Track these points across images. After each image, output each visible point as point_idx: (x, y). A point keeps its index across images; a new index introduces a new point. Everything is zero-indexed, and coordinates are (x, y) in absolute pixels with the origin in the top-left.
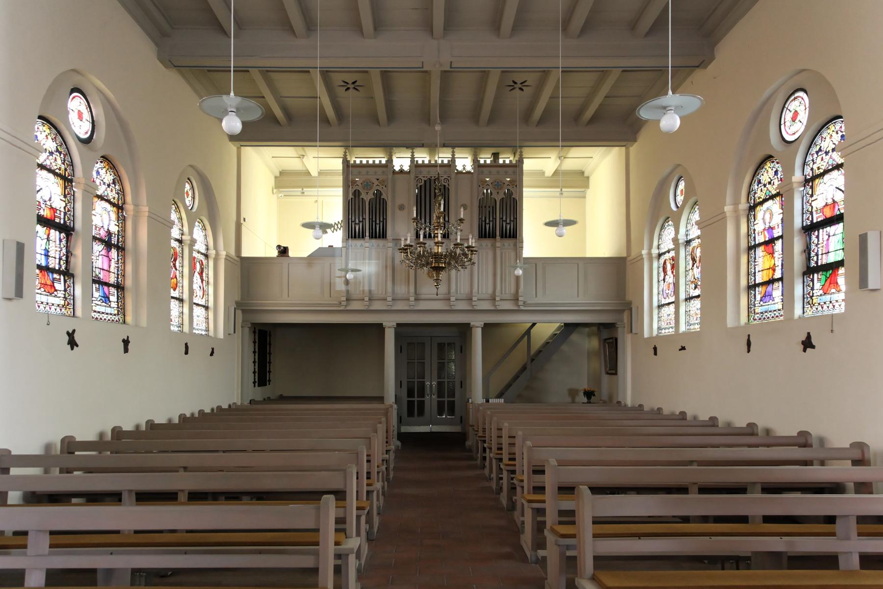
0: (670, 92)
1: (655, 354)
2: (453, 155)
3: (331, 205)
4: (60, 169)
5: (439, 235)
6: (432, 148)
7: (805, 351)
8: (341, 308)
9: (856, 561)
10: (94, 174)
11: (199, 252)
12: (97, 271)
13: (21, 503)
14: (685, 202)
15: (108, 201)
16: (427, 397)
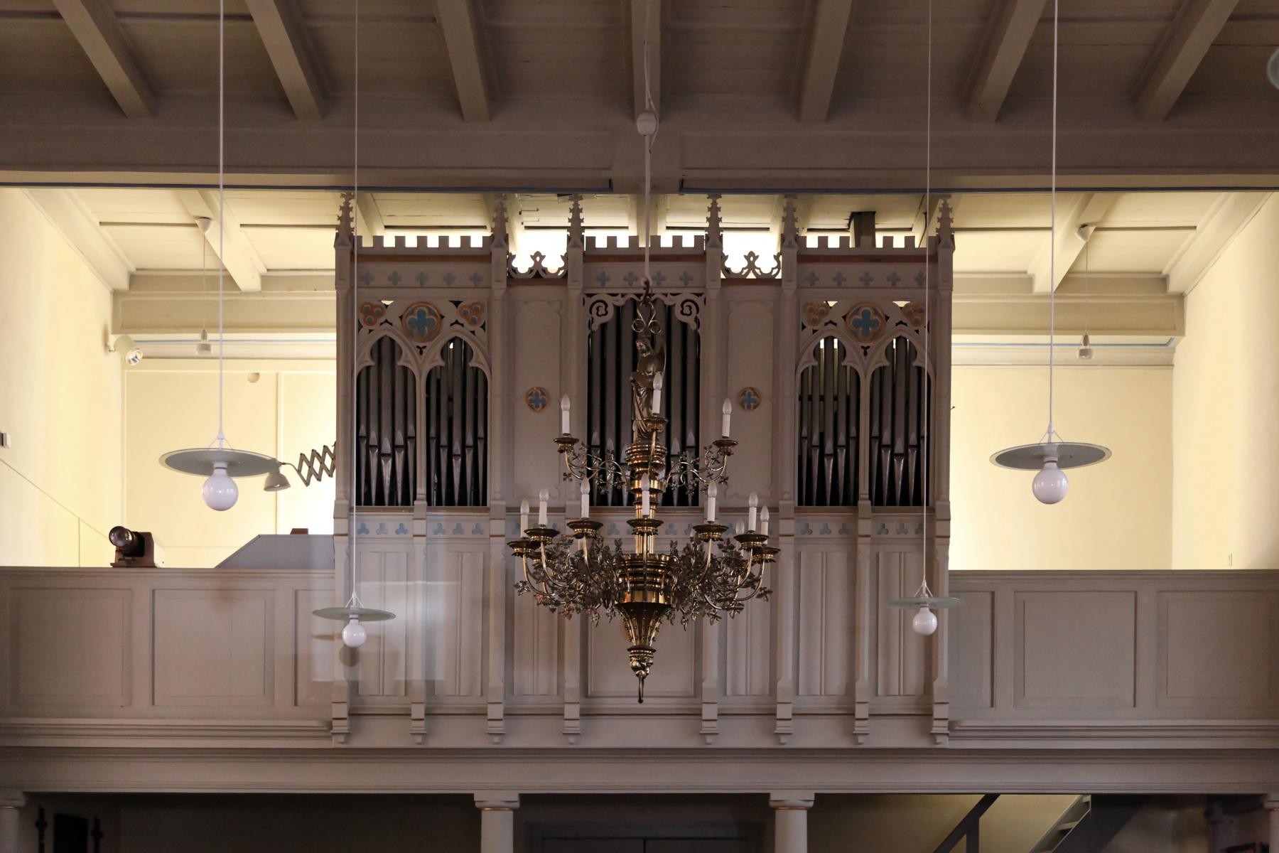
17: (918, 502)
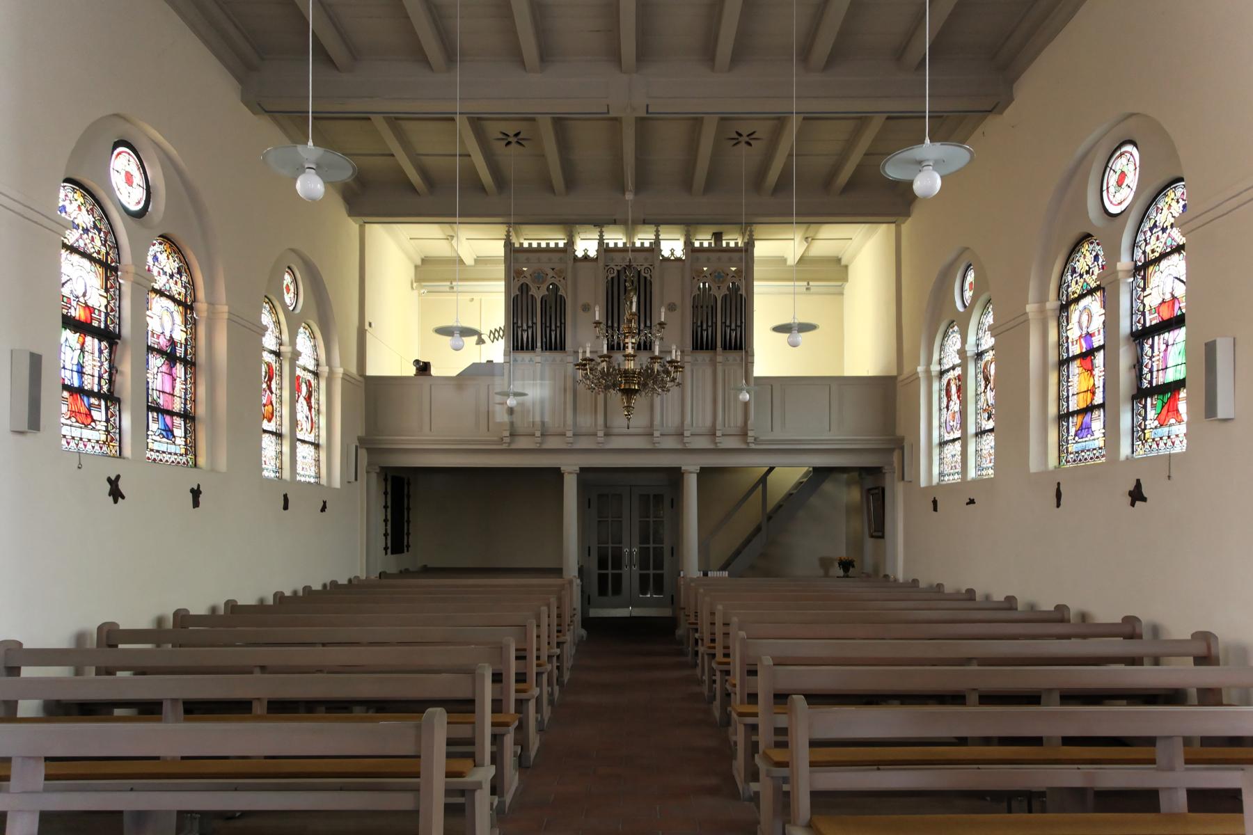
0: (927, 140)
1: (935, 509)
2: (657, 235)
3: (489, 306)
4: (99, 253)
5: (630, 345)
6: (630, 224)
7: (1133, 505)
8: (504, 446)
9: (1182, 798)
10: (150, 259)
11: (305, 369)
12: (155, 394)
13: (41, 715)
14: (975, 298)
16: (625, 570)
17: (741, 348)
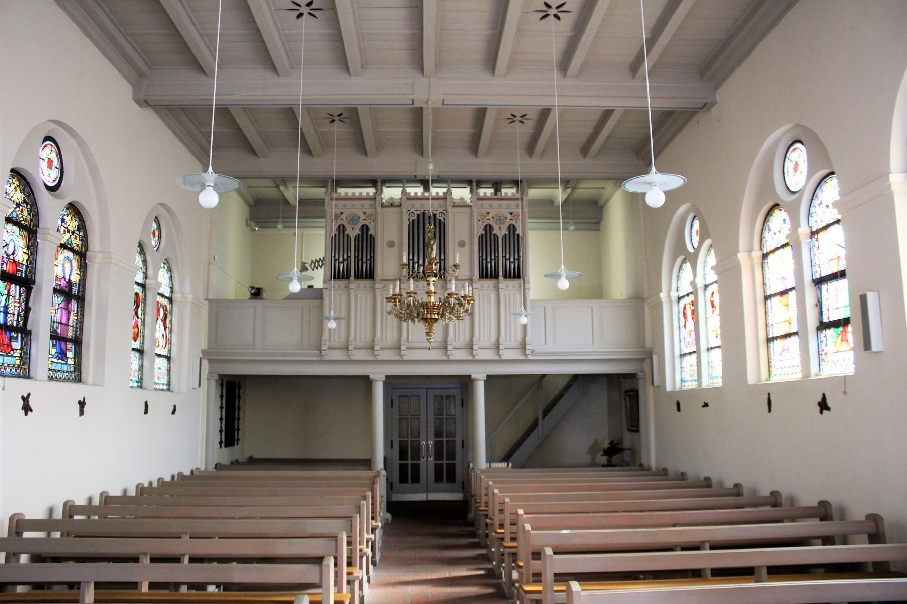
1: (679, 410)
4: (26, 220)
11: (162, 296)
12: (56, 325)
14: (701, 243)
15: (71, 249)
16: (423, 460)
17: (519, 277)
